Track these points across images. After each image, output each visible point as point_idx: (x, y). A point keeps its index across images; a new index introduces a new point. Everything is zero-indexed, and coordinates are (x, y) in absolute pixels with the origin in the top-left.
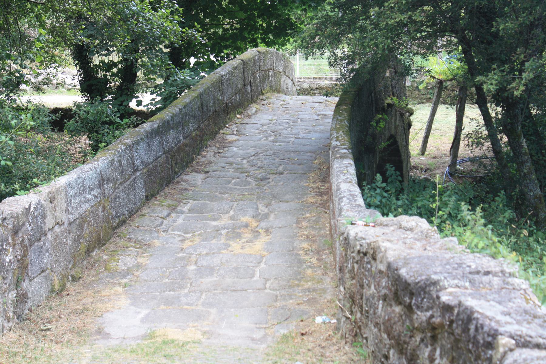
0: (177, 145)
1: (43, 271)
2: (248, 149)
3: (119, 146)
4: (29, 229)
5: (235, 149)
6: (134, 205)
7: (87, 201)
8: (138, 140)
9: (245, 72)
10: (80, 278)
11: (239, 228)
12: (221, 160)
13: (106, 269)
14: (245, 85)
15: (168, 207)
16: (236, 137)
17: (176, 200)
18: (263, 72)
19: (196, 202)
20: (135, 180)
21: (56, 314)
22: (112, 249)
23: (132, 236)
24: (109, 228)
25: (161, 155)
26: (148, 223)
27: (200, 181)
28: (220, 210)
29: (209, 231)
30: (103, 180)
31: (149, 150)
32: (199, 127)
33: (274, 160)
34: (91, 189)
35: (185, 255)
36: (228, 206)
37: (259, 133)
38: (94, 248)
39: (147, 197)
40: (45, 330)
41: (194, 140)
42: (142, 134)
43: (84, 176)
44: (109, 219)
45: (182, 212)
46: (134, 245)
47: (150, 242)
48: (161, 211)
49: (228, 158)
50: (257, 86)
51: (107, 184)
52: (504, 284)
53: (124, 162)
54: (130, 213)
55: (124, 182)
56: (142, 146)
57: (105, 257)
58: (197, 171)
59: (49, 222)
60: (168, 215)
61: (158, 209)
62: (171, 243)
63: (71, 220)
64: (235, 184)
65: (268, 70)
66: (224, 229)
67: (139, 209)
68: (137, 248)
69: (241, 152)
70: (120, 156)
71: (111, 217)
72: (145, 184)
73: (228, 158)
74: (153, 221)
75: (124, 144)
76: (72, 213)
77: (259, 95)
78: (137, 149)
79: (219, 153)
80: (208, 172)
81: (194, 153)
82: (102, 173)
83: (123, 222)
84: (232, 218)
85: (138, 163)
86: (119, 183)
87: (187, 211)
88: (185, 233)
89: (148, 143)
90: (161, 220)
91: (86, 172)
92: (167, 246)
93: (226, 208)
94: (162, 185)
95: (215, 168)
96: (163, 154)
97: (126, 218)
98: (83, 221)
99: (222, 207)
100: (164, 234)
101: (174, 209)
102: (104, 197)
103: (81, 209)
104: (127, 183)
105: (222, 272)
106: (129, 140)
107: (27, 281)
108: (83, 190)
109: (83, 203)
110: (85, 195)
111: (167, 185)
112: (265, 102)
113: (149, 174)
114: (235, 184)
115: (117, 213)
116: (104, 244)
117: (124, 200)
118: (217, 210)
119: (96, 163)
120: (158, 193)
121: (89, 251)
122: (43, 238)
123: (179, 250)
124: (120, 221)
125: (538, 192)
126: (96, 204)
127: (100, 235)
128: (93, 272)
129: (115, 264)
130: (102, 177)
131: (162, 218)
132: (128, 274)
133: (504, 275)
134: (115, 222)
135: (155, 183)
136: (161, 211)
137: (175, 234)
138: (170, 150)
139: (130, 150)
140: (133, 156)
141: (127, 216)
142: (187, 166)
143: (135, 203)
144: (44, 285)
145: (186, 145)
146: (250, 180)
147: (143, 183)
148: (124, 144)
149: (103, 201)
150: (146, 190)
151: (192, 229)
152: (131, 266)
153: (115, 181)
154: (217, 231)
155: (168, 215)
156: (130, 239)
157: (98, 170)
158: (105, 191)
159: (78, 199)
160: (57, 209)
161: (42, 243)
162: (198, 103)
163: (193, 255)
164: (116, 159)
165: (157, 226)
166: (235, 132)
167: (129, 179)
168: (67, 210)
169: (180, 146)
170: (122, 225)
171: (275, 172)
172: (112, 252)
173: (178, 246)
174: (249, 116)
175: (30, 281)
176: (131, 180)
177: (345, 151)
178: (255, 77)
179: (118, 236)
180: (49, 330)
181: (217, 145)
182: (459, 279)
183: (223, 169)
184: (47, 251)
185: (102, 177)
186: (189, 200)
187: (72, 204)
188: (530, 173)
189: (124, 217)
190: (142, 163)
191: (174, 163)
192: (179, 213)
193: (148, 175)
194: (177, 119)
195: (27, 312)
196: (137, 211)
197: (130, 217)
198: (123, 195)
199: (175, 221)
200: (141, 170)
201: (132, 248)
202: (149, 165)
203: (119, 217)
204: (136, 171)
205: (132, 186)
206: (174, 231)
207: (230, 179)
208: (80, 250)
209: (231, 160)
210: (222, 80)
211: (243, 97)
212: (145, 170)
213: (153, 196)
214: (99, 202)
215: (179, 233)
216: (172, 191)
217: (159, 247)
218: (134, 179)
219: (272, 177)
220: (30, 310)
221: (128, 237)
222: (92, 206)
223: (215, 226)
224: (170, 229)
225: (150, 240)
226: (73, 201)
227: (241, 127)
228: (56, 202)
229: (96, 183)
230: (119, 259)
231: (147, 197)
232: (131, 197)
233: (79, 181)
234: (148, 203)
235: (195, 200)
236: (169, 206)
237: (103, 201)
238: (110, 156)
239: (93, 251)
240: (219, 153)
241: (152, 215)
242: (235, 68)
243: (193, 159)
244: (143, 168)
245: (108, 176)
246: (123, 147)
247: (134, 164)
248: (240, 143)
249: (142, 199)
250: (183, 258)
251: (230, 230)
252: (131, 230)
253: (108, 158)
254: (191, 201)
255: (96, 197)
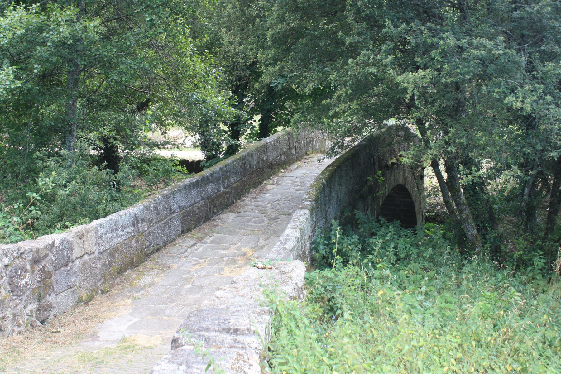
0: (215, 193)
1: (71, 288)
4: (54, 259)
8: (175, 191)
9: (290, 140)
10: (108, 291)
11: (238, 256)
14: (290, 149)
18: (308, 140)
21: (73, 319)
22: (141, 270)
23: (159, 261)
32: (241, 179)
33: (290, 204)
34: (124, 227)
37: (291, 183)
38: (127, 268)
40: (56, 332)
41: (237, 188)
44: (142, 248)
45: (205, 243)
50: (301, 149)
51: (142, 223)
52: (235, 343)
53: (160, 207)
57: (134, 276)
59: (77, 252)
62: (185, 267)
63: (102, 250)
64: (254, 222)
65: (313, 138)
67: (174, 240)
69: (271, 197)
70: (156, 203)
72: (182, 222)
73: (259, 202)
76: (102, 245)
77: (303, 155)
80: (240, 212)
81: (234, 198)
83: (158, 250)
98: (114, 251)
101: (200, 240)
105: (206, 290)
107: (53, 295)
108: (116, 229)
110: (117, 232)
111: (204, 222)
112: (307, 161)
114: (254, 222)
120: (194, 228)
122: (70, 264)
124: (154, 249)
125: (475, 232)
128: (120, 287)
132: (143, 289)
133: (250, 332)
137: (192, 260)
138: (208, 197)
142: (226, 208)
144: (71, 297)
150: (182, 227)
153: (150, 221)
159: (109, 235)
161: (68, 268)
165: (181, 253)
169: (220, 194)
170: (157, 251)
171: (285, 213)
174: (291, 171)
175: (56, 295)
177: (309, 203)
178: (300, 143)
180: (59, 332)
182: (195, 338)
184: (75, 273)
187: (103, 239)
188: (468, 218)
190: (179, 207)
191: (212, 207)
195: (52, 317)
203: (153, 246)
205: (168, 224)
208: (111, 271)
209: (260, 203)
211: (287, 157)
213: (189, 230)
219: (282, 217)
220: (55, 316)
222: (125, 240)
226: (104, 236)
228: (85, 238)
232: (167, 232)
239: (125, 271)
243: (233, 203)
245: (143, 217)
247: (170, 209)
248: (272, 191)
250: (186, 279)
255: (128, 233)
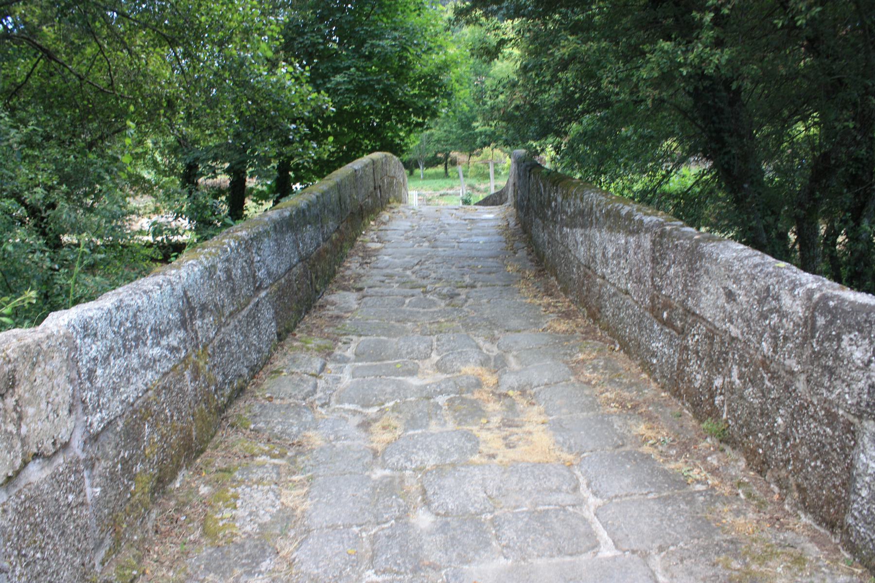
0: (316, 249)
2: (404, 257)
3: (226, 241)
5: (386, 258)
6: (259, 352)
7: (149, 364)
12: (375, 271)
13: (205, 533)
15: (319, 352)
16: (379, 245)
17: (328, 338)
19: (363, 338)
20: (257, 306)
22: (219, 463)
24: (210, 412)
25: (297, 263)
26: (289, 389)
27: (354, 302)
28: (412, 352)
29: (413, 399)
30: (192, 309)
31: (279, 252)
32: (338, 227)
34: (159, 333)
35: (387, 472)
36: (425, 345)
38: (179, 467)
39: (279, 335)
42: (267, 224)
43: (140, 301)
44: (209, 392)
45: (345, 360)
46: (267, 448)
47: (300, 437)
48: (309, 360)
49: (382, 268)
53: (237, 272)
54: (252, 370)
55: (238, 311)
56: (268, 244)
57: (204, 490)
58: (346, 289)
60: (323, 368)
61: (302, 356)
63: (97, 427)
66: (441, 393)
67: (268, 360)
68: (274, 457)
70: (228, 260)
71: (213, 388)
72: (276, 313)
73: (382, 268)
74: (298, 385)
75: (236, 238)
76: (98, 407)
78: (259, 249)
79: (367, 263)
82: (189, 294)
83: (241, 391)
84: (440, 367)
85: (261, 274)
86: (227, 314)
87: (353, 357)
88: (363, 406)
89: (276, 240)
90: (312, 381)
91: (145, 292)
92: (339, 444)
93: (422, 348)
94: (300, 312)
95: (370, 282)
96: (300, 261)
97: (245, 381)
99: (415, 347)
100: (323, 411)
101: (329, 354)
102: (197, 346)
103: (132, 387)
104: (244, 313)
106: (244, 233)
108: (137, 339)
109: (136, 371)
110: (141, 349)
111: (307, 312)
113: (281, 294)
115: (226, 376)
116: (202, 451)
117: (239, 346)
118: (408, 353)
119: (173, 272)
120: (295, 326)
121: (162, 483)
123: (369, 459)
124: (233, 390)
126: (175, 367)
127: (190, 435)
129: (227, 514)
130: (188, 301)
131: (313, 375)
134: (222, 395)
135: (290, 309)
136: (309, 360)
139: (248, 249)
140: (252, 262)
141: (247, 377)
143: (261, 348)
145: (326, 251)
146: (431, 297)
147: (272, 311)
148: (236, 238)
149: (193, 357)
150: (278, 324)
151: (376, 396)
152: (267, 519)
153: (218, 310)
154: (428, 398)
155: (323, 368)
156: (257, 431)
157: (178, 288)
158: (196, 332)
159: (117, 365)
160: (30, 411)
162: (334, 196)
163: (408, 473)
164: (219, 265)
166: (376, 240)
167: (246, 305)
168: (77, 405)
170: (238, 396)
172: (220, 474)
173: (361, 442)
176: (250, 306)
179: (232, 426)
181: (361, 254)
183: (382, 284)
185: (188, 301)
186: (350, 337)
187: (99, 383)
189: (241, 381)
190: (269, 274)
191: (314, 277)
192: (339, 361)
193: (280, 297)
194: (315, 211)
196: (265, 364)
197: (253, 377)
198: (236, 337)
199: (338, 380)
200: (266, 288)
201: (264, 458)
202: (280, 278)
203: (231, 382)
204: (258, 289)
205: (253, 317)
206: (341, 403)
207: (400, 297)
208: (133, 495)
209: (388, 271)
210: (356, 176)
212: (274, 288)
213: (288, 331)
214: (183, 361)
215: (352, 407)
216: (317, 322)
217: (322, 449)
218: (257, 305)
221: (252, 426)
222: (165, 374)
223: (422, 388)
224: (333, 399)
225: (299, 432)
226: (99, 372)
227: (380, 233)
229: (174, 317)
230: (236, 498)
231: (279, 335)
232: (253, 339)
233: (121, 315)
234: (282, 346)
235: (361, 336)
236: (320, 349)
237: (193, 357)
238: (207, 259)
239: (173, 478)
240: (367, 263)
241: (294, 370)
242: (366, 166)
243: (335, 273)
244: (271, 285)
245: (203, 300)
246: (232, 244)
247: (254, 277)
249: (272, 340)
251: (452, 395)
252: (257, 409)
253: (201, 263)
254: (355, 338)
255: (173, 349)
